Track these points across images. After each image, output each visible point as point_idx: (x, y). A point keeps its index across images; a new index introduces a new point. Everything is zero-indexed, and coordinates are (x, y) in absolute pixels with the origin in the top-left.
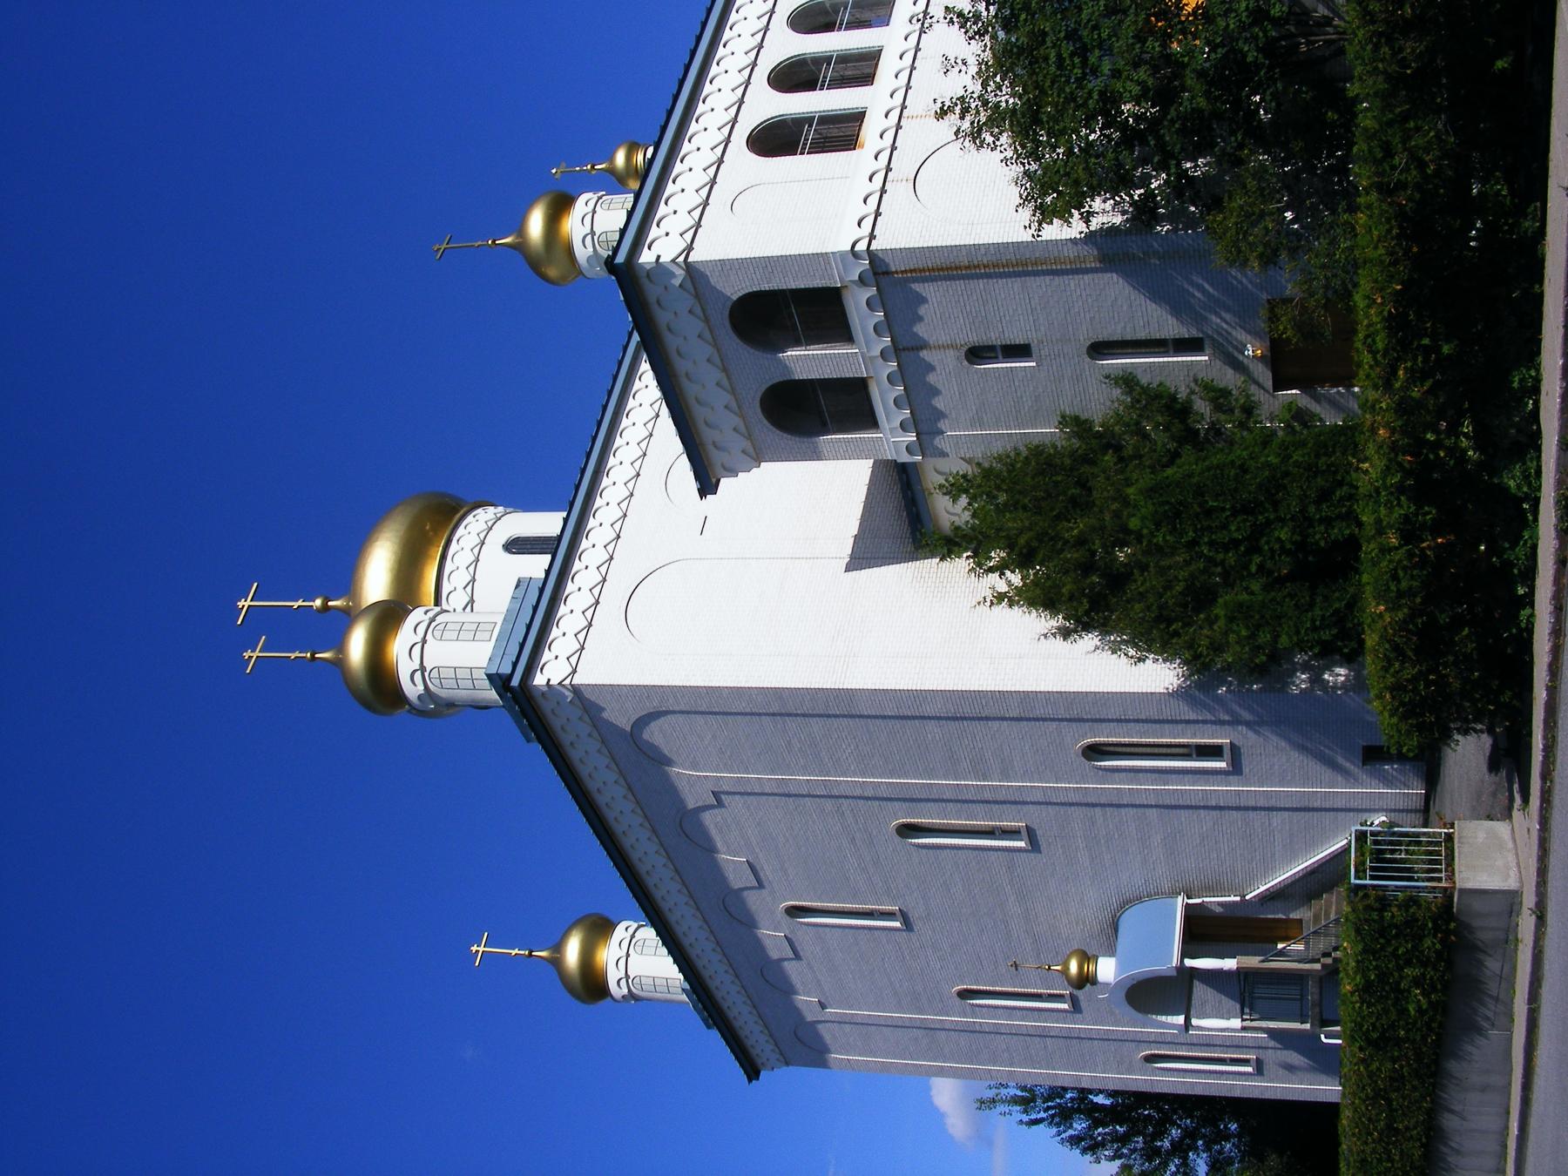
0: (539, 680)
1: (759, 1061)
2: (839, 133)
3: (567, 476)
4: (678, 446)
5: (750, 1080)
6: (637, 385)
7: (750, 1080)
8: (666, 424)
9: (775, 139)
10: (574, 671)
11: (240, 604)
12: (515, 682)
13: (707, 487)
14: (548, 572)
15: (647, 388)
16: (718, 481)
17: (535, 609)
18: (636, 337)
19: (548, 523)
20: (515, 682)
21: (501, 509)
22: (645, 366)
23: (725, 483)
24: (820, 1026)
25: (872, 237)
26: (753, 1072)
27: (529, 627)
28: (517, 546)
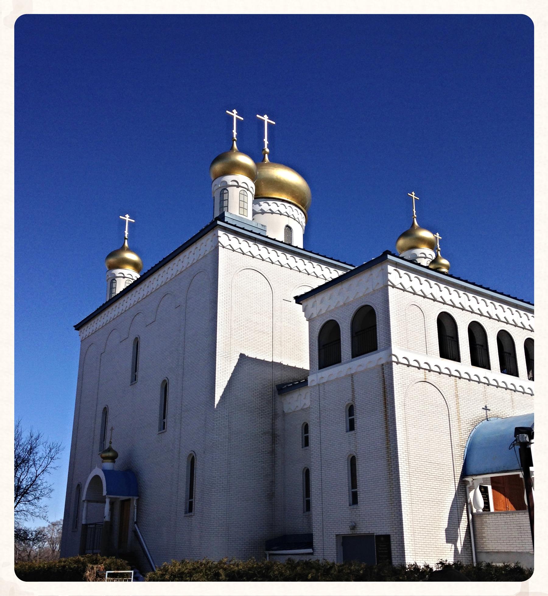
0: (220, 233)
1: (82, 330)
2: (448, 348)
3: (313, 249)
4: (315, 286)
5: (74, 326)
6: (332, 269)
7: (74, 326)
8: (322, 282)
9: (446, 325)
10: (224, 247)
11: (235, 111)
12: (219, 223)
13: (299, 299)
14: (296, 247)
15: (335, 274)
16: (301, 304)
17: (251, 232)
18: (352, 268)
19: (298, 241)
20: (219, 223)
21: (304, 225)
22: (341, 273)
23: (300, 307)
24: (393, 356)
25: (398, 363)
26: (78, 327)
27: (243, 229)
28: (288, 228)
